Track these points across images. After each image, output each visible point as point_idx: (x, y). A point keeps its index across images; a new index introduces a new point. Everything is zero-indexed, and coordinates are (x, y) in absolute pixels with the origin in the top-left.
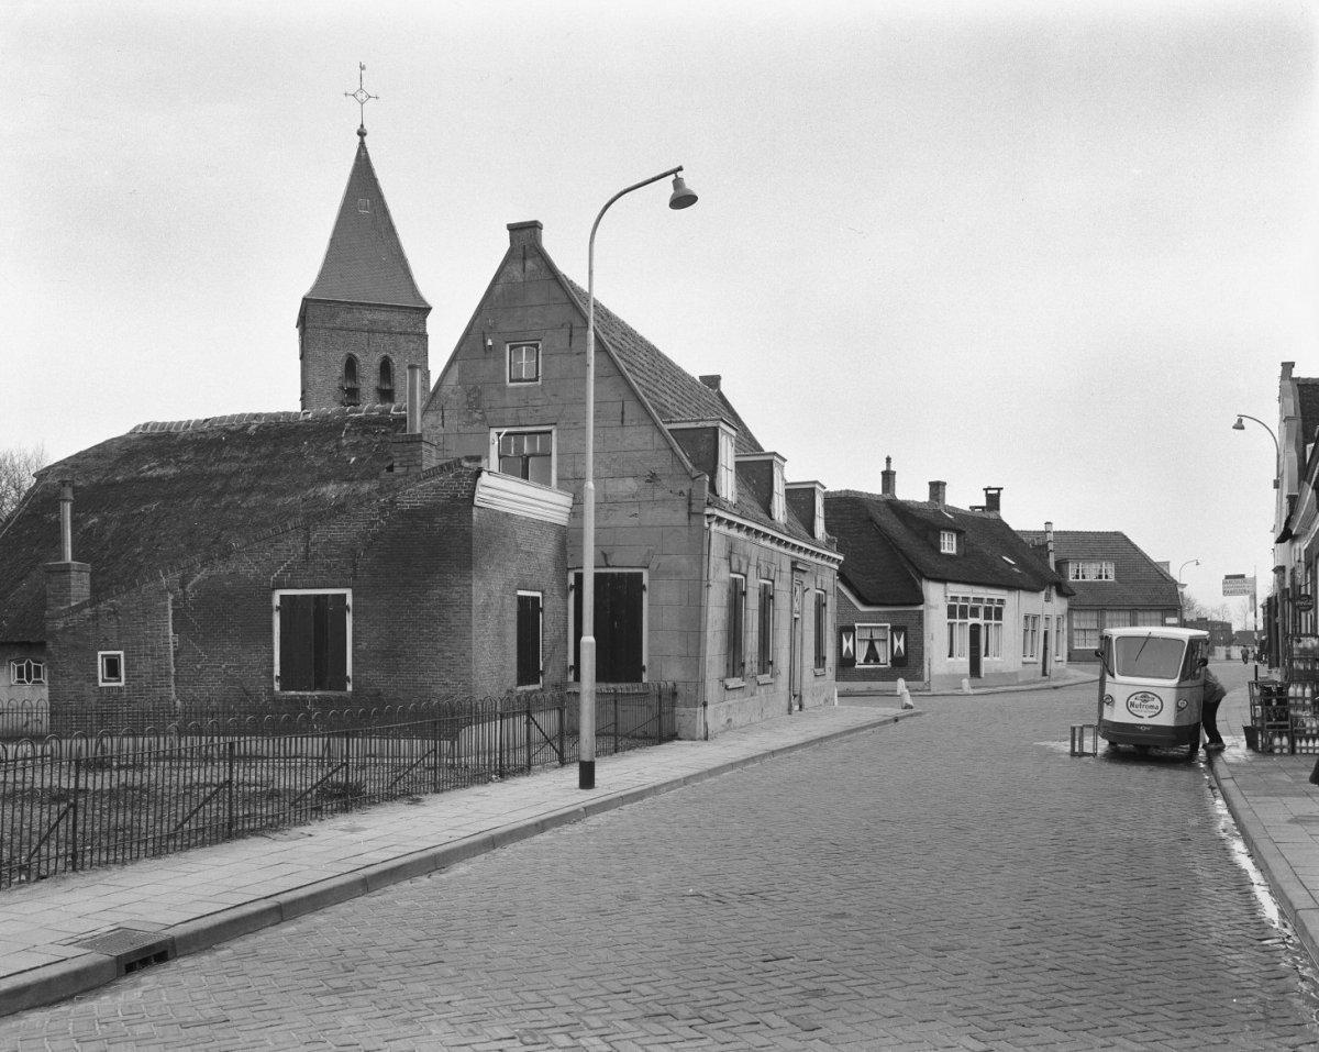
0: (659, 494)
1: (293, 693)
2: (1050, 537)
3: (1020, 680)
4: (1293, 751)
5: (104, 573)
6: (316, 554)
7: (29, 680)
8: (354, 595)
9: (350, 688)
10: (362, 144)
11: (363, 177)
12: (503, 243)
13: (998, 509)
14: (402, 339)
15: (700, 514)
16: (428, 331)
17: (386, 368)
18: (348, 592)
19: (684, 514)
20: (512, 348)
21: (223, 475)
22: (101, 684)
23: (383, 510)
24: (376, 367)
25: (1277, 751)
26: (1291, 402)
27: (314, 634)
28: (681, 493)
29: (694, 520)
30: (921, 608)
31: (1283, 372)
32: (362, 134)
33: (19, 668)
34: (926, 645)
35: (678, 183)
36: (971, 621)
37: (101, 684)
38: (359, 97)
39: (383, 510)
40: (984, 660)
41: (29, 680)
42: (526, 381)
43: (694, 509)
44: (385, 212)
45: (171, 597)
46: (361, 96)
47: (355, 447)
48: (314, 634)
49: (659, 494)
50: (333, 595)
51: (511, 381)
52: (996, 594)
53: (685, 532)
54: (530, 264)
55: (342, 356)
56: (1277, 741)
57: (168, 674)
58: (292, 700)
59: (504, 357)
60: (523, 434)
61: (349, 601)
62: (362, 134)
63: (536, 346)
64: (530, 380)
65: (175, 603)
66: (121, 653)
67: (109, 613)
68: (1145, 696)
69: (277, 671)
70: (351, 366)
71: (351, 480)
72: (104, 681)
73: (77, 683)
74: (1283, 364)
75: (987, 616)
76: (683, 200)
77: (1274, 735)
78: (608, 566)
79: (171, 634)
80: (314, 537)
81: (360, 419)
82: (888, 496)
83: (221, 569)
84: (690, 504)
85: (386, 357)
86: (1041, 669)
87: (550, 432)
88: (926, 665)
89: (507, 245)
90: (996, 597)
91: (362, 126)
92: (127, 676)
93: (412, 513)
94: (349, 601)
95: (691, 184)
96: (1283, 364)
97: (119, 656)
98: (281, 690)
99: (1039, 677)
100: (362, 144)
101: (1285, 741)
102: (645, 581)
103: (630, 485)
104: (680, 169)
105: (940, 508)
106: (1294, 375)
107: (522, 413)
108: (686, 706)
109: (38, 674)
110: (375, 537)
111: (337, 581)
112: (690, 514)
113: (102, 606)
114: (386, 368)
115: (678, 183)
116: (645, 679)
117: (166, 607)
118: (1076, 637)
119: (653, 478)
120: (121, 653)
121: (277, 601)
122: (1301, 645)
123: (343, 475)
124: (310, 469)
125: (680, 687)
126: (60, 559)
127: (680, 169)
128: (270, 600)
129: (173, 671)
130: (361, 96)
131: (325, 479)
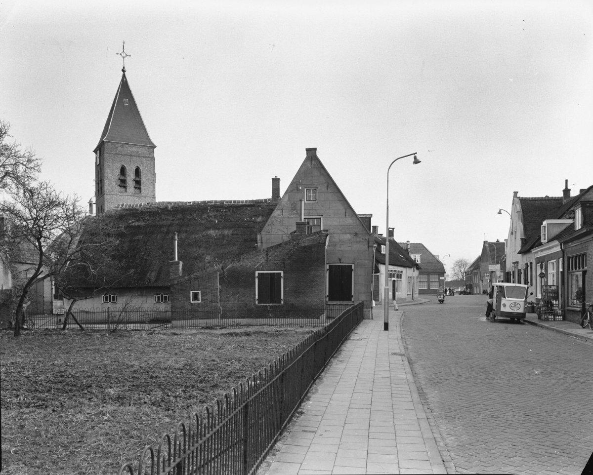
0: (358, 240)
1: (262, 304)
2: (409, 247)
3: (407, 301)
4: (554, 320)
5: (132, 262)
6: (271, 260)
7: (110, 301)
8: (284, 273)
9: (282, 302)
10: (124, 76)
11: (124, 89)
12: (304, 155)
13: (393, 236)
14: (144, 159)
15: (372, 246)
16: (155, 156)
17: (137, 172)
18: (282, 272)
19: (367, 246)
20: (307, 190)
21: (165, 226)
22: (192, 302)
23: (294, 246)
24: (134, 171)
25: (550, 320)
26: (519, 207)
27: (270, 285)
28: (366, 240)
29: (370, 248)
30: (378, 274)
31: (514, 195)
32: (123, 71)
33: (106, 297)
34: (380, 288)
35: (415, 158)
36: (393, 279)
37: (192, 302)
38: (125, 54)
39: (294, 246)
40: (397, 293)
41: (110, 301)
42: (312, 201)
43: (370, 245)
44: (135, 105)
45: (218, 273)
46: (124, 55)
47: (215, 216)
48: (270, 285)
49: (358, 240)
50: (277, 273)
51: (307, 201)
52: (400, 269)
53: (367, 252)
54: (313, 162)
55: (119, 166)
56: (550, 317)
57: (217, 298)
58: (263, 307)
59: (304, 193)
60: (310, 218)
61: (282, 275)
62: (123, 71)
63: (316, 189)
64: (313, 201)
65: (220, 275)
66: (200, 291)
67: (195, 278)
68: (515, 304)
69: (257, 297)
70: (123, 170)
71: (219, 229)
72: (193, 301)
73: (182, 301)
74: (514, 192)
75: (397, 277)
76: (416, 162)
77: (549, 315)
78: (341, 263)
79: (218, 285)
80: (270, 254)
81: (212, 205)
82: (120, 200)
83: (237, 264)
84: (369, 243)
85: (137, 167)
86: (411, 297)
87: (320, 218)
88: (380, 295)
89: (306, 156)
90: (397, 270)
91: (124, 68)
92: (202, 299)
93: (305, 247)
94: (282, 275)
95: (418, 158)
96: (514, 192)
97: (199, 292)
98: (258, 303)
99: (411, 300)
100: (124, 76)
101: (552, 317)
102: (353, 267)
103: (348, 236)
104: (416, 153)
105: (377, 236)
106: (518, 196)
107: (311, 212)
108: (367, 308)
109: (166, 299)
110: (292, 254)
111: (278, 268)
112: (369, 246)
113: (192, 276)
114: (137, 172)
115: (415, 158)
116: (353, 300)
117: (217, 276)
118: (431, 284)
119: (356, 234)
120: (200, 291)
121: (257, 275)
122: (551, 289)
123: (215, 227)
124: (201, 224)
125: (365, 302)
126: (173, 260)
127: (416, 153)
128: (254, 274)
129: (219, 297)
130: (124, 55)
131: (208, 228)
